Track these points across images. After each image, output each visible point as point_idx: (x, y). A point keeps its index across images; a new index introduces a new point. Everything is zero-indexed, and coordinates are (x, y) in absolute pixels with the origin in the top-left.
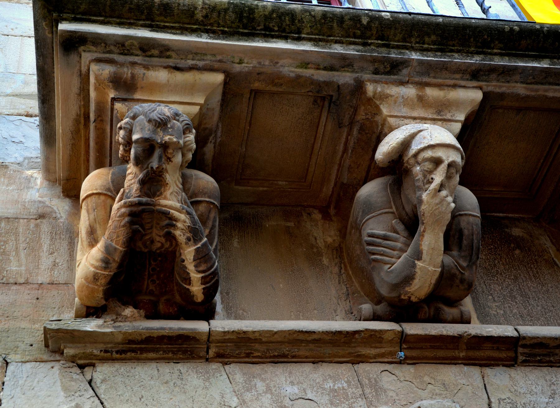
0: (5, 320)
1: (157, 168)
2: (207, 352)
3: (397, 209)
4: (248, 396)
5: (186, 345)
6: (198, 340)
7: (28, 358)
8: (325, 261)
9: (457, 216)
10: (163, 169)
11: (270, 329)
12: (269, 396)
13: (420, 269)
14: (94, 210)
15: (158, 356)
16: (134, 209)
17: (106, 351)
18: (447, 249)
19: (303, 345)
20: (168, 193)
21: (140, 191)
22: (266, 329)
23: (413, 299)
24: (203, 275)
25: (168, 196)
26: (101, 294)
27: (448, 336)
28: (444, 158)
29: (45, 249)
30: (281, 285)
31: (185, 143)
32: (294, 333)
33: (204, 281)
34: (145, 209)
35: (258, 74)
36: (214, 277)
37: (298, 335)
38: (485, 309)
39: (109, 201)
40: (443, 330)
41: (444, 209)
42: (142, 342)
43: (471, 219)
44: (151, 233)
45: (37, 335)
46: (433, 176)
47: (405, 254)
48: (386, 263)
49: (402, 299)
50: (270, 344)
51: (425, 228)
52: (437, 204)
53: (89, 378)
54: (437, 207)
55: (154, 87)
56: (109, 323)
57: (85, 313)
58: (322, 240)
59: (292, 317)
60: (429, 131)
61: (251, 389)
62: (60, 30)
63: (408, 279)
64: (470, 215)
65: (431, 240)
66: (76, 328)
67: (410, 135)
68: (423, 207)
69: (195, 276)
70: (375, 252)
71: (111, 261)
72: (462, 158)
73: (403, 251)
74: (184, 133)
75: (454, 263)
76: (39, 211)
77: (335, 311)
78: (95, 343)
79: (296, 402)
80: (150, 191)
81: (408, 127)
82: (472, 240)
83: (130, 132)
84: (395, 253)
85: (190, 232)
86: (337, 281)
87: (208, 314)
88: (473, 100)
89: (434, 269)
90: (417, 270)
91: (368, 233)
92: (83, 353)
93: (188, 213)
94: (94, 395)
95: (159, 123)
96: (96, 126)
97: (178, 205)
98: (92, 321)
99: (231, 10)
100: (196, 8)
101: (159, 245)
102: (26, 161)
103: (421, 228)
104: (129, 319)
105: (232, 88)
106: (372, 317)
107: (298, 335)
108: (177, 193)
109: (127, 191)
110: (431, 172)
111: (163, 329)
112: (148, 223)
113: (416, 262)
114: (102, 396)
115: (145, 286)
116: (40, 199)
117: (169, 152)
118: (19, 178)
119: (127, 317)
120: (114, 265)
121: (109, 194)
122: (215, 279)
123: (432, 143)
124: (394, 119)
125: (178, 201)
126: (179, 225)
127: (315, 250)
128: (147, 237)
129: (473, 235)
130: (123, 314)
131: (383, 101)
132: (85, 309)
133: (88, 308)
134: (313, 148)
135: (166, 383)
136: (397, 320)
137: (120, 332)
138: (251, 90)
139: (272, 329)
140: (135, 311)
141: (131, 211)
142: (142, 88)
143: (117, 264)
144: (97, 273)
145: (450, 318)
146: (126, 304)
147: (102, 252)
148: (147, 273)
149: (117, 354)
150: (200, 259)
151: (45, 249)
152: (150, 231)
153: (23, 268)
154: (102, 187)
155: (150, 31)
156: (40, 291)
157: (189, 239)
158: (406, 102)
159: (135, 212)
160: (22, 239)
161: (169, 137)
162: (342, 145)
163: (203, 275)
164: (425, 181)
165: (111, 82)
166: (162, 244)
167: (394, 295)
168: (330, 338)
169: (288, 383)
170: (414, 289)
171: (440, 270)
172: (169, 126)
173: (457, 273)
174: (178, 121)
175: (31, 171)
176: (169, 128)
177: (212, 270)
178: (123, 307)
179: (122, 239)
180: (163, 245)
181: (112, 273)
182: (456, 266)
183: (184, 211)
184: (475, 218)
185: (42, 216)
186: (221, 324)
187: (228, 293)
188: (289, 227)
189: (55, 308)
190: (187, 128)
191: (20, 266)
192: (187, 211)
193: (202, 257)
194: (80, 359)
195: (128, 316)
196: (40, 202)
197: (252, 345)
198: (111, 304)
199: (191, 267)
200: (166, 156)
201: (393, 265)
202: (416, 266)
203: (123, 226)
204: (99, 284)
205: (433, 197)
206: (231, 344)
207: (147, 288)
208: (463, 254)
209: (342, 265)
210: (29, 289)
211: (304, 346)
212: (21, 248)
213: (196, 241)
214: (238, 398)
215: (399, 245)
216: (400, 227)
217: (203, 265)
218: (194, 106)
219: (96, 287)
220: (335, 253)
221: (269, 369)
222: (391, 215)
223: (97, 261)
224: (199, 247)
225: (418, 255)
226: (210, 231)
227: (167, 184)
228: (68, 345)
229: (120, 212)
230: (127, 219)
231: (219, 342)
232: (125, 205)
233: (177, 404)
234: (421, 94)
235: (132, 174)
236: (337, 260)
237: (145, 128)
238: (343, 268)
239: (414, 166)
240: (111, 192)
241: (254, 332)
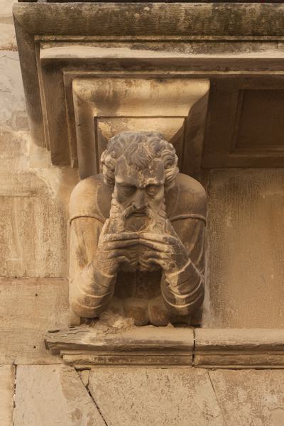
0: (10, 319)
2: (193, 360)
4: (229, 406)
7: (33, 360)
12: (249, 405)
15: (147, 363)
16: (120, 243)
17: (100, 359)
20: (151, 226)
22: (249, 343)
24: (187, 295)
25: (151, 229)
39: (97, 222)
45: (38, 336)
53: (86, 382)
55: (137, 102)
61: (233, 397)
62: (44, 60)
79: (275, 411)
87: (192, 319)
93: (171, 243)
94: (91, 400)
96: (81, 129)
99: (216, 18)
100: (178, 20)
102: (15, 116)
105: (217, 87)
109: (112, 223)
114: (98, 402)
120: (103, 290)
121: (96, 216)
135: (154, 390)
139: (254, 343)
141: (117, 245)
142: (124, 104)
144: (89, 297)
151: (39, 236)
153: (21, 259)
155: (131, 48)
160: (17, 223)
163: (187, 295)
165: (94, 101)
169: (269, 391)
172: (150, 168)
174: (159, 157)
185: (33, 193)
186: (207, 335)
191: (18, 256)
194: (78, 364)
195: (119, 327)
199: (175, 290)
210: (28, 285)
214: (220, 407)
219: (88, 307)
221: (250, 374)
230: (113, 252)
233: (164, 412)
240: (98, 213)
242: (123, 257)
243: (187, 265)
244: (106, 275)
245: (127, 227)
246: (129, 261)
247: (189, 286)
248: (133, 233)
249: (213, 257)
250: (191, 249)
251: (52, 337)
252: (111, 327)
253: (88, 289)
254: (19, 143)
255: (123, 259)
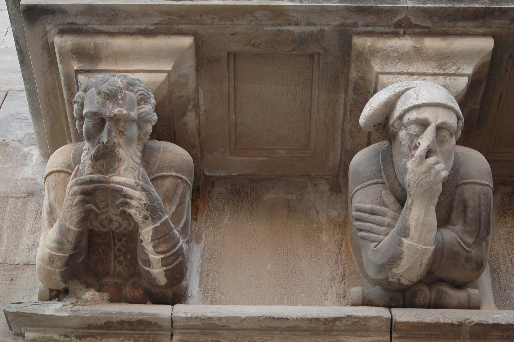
1: (107, 142)
3: (388, 178)
5: (149, 330)
6: (160, 326)
8: (324, 238)
9: (460, 185)
10: (115, 143)
11: (237, 315)
13: (408, 247)
14: (54, 188)
18: (444, 221)
19: (277, 332)
20: (122, 169)
21: (92, 168)
22: (233, 315)
23: (404, 281)
24: (163, 256)
26: (59, 276)
27: (445, 325)
28: (431, 119)
29: (27, 229)
30: (269, 266)
31: (139, 115)
32: (265, 320)
33: (165, 262)
34: (97, 187)
35: (232, 34)
36: (177, 259)
37: (270, 322)
38: (505, 291)
40: (441, 316)
41: (432, 178)
42: (102, 327)
43: (478, 187)
44: (107, 212)
46: (420, 141)
47: (393, 231)
48: (372, 241)
49: (391, 282)
50: (240, 332)
51: (412, 201)
52: (424, 173)
54: (424, 176)
56: (68, 307)
57: (48, 296)
58: (325, 214)
59: (275, 301)
60: (418, 88)
63: (395, 259)
64: (477, 183)
65: (420, 215)
66: (33, 312)
67: (395, 95)
68: (408, 177)
69: (155, 257)
70: (361, 228)
71: (65, 242)
72: (459, 118)
73: (391, 226)
74: (139, 104)
75: (456, 239)
76: (29, 189)
77: (325, 295)
78: (55, 327)
80: (103, 167)
81: (395, 85)
82: (480, 212)
83: (82, 106)
84: (383, 229)
85: (147, 210)
86: (334, 261)
87: (177, 297)
88: (482, 50)
89: (424, 247)
90: (404, 249)
91: (355, 208)
92: (43, 337)
93: (144, 190)
95: (108, 95)
97: (132, 181)
98: (51, 305)
101: (116, 224)
102: (27, 137)
103: (409, 201)
104: (90, 303)
106: (361, 302)
107: (270, 322)
108: (133, 168)
110: (417, 136)
111: (121, 313)
112: (103, 201)
113: (403, 239)
115: (113, 267)
116: (32, 176)
117: (120, 125)
118: (17, 156)
119: (87, 301)
120: (69, 247)
122: (179, 260)
123: (417, 103)
124: (387, 76)
125: (135, 177)
126: (134, 203)
127: (315, 226)
128: (103, 216)
129: (480, 207)
130: (83, 297)
131: (374, 56)
132: (48, 292)
133: (51, 290)
134: (310, 111)
136: (389, 306)
137: (77, 316)
138: (228, 53)
139: (240, 315)
140: (97, 294)
141: (83, 189)
142: (106, 57)
143: (72, 246)
144: (52, 255)
145: (455, 302)
146: (88, 286)
147: (57, 233)
148: (113, 254)
149: (77, 339)
150: (159, 238)
151: (27, 229)
152: (106, 210)
154: (63, 165)
156: (15, 272)
157: (146, 218)
158: (402, 57)
159: (87, 191)
161: (119, 109)
162: (342, 108)
163: (163, 256)
164: (412, 147)
166: (120, 223)
167: (381, 276)
168: (307, 325)
170: (401, 271)
171: (432, 248)
172: (120, 97)
173: (461, 251)
174: (132, 91)
175: (29, 148)
176: (120, 100)
177: (175, 250)
178: (84, 290)
179: (75, 219)
180: (120, 224)
181: (67, 255)
182: (459, 242)
183: (139, 188)
184: (483, 187)
187: (207, 275)
188: (289, 200)
189: (26, 290)
190: (141, 98)
192: (142, 188)
193: (162, 236)
195: (89, 299)
196: (32, 179)
197: (220, 332)
198: (74, 286)
199: (149, 248)
200: (118, 129)
201: (380, 242)
202: (403, 244)
203: (76, 205)
204: (55, 266)
205: (418, 165)
206: (197, 331)
207: (115, 270)
208: (468, 229)
209: (344, 243)
211: (279, 334)
212: (5, 227)
213: (154, 220)
215: (387, 220)
216: (390, 199)
217: (162, 246)
218: (161, 74)
219: (52, 269)
220: (337, 229)
222: (380, 185)
223: (52, 242)
224: (158, 226)
225: (405, 232)
226: (177, 208)
227: (121, 159)
228: (28, 329)
229: (72, 191)
230: (78, 198)
231: (183, 329)
232: (76, 184)
234: (418, 46)
235: (87, 150)
236: (338, 237)
237: (94, 100)
238: (344, 246)
239: (400, 129)
241: (220, 319)
242: (91, 205)
243: (163, 220)
244: (72, 227)
245: (95, 169)
246: (98, 211)
247: (165, 245)
248: (102, 176)
249: (206, 249)
250: (172, 212)
251: (13, 307)
252: (80, 298)
253: (54, 245)
254: (26, 156)
255: (90, 207)
